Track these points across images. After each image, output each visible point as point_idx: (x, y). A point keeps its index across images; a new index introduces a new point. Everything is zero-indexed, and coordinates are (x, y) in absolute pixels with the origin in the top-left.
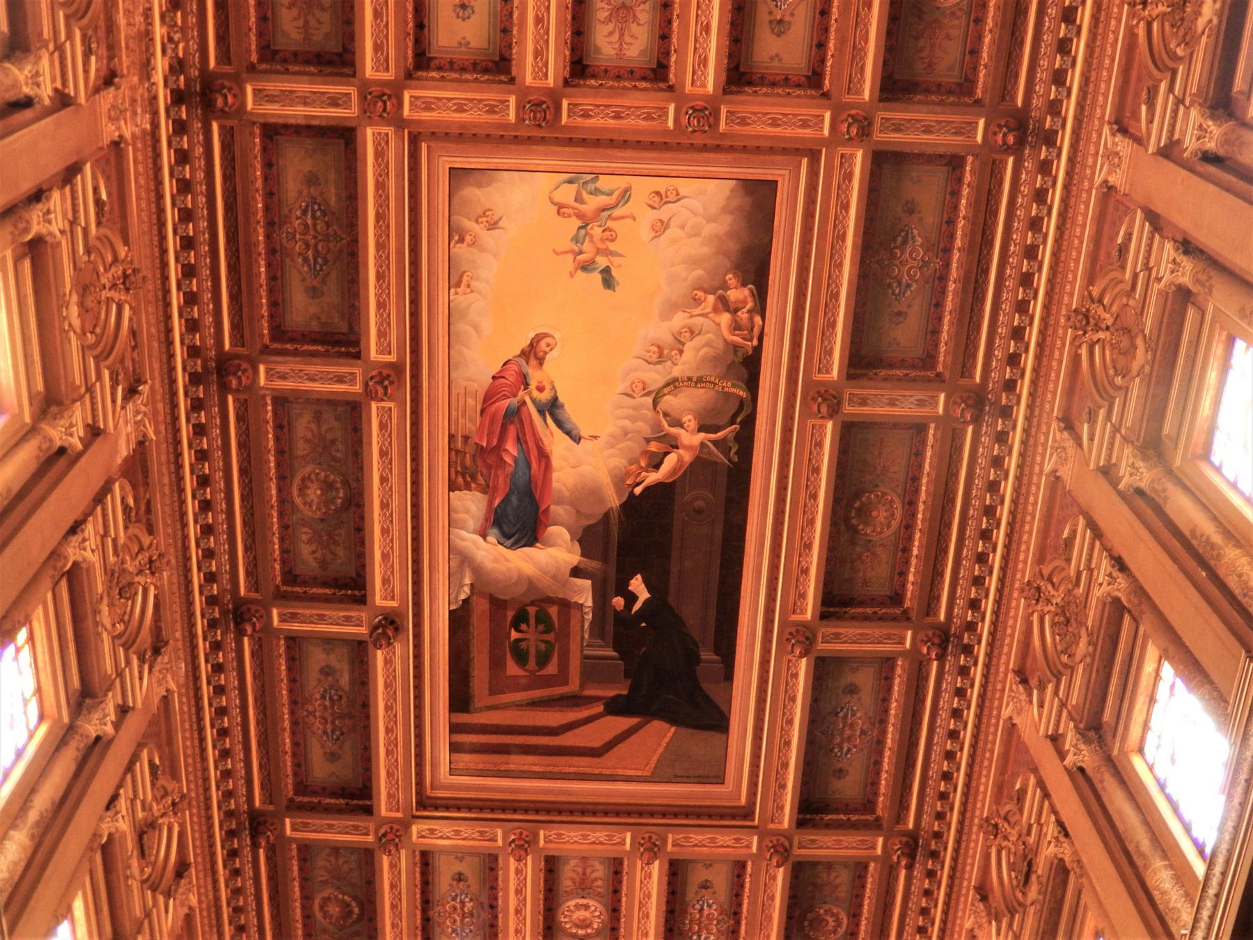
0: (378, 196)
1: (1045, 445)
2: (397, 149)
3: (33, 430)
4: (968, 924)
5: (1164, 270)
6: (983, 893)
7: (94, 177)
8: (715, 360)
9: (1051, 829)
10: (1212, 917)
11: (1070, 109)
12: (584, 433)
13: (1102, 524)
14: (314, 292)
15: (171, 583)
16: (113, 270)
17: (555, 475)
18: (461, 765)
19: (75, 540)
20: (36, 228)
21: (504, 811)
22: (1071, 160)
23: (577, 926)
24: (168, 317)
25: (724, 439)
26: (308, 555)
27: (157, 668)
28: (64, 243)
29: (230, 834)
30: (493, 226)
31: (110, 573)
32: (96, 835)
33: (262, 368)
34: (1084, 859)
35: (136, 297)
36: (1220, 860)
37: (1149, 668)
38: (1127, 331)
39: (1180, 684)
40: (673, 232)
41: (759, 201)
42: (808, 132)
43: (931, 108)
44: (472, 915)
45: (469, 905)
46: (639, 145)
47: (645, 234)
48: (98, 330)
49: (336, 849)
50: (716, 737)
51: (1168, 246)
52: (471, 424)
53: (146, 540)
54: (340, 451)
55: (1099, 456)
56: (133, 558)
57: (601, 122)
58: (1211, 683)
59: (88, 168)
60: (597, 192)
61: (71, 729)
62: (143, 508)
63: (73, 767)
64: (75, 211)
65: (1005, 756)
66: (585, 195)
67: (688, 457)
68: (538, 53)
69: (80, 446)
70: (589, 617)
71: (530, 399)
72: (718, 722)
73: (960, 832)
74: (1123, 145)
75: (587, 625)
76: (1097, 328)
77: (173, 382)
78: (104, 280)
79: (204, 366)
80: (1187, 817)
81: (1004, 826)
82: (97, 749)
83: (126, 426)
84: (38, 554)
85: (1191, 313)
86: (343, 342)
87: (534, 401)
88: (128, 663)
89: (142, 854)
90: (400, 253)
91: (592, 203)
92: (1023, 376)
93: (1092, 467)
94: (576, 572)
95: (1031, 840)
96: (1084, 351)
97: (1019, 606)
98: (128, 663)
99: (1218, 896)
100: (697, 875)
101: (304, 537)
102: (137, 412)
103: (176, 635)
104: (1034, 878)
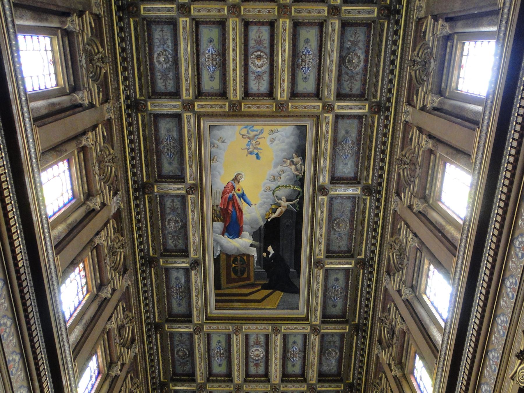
0: (188, 134)
1: (391, 201)
2: (193, 120)
3: (84, 203)
4: (376, 352)
5: (423, 144)
6: (380, 342)
7: (102, 129)
8: (291, 180)
9: (399, 320)
10: (448, 340)
11: (394, 100)
12: (252, 203)
13: (409, 224)
14: (170, 164)
15: (129, 252)
16: (109, 157)
17: (244, 216)
18: (219, 306)
19: (98, 237)
20: (84, 143)
21: (232, 320)
22: (395, 115)
23: (256, 357)
24: (127, 172)
25: (294, 203)
27: (125, 278)
28: (93, 148)
29: (148, 330)
30: (223, 142)
31: (109, 248)
32: (105, 328)
33: (155, 187)
34: (409, 328)
35: (117, 165)
36: (449, 320)
37: (426, 267)
38: (414, 164)
39: (436, 271)
40: (276, 142)
41: (302, 131)
42: (315, 110)
43: (351, 101)
44: (223, 354)
45: (222, 351)
46: (265, 116)
47: (268, 143)
48: (105, 175)
49: (181, 334)
50: (296, 295)
51: (424, 137)
52: (218, 201)
53: (121, 238)
54: (179, 211)
55: (407, 202)
56: (117, 244)
57: (254, 109)
58: (445, 268)
59: (100, 125)
60: (253, 131)
61: (97, 296)
62: (120, 229)
63: (97, 307)
64: (96, 138)
65: (384, 298)
66: (250, 132)
67: (284, 209)
68: (234, 90)
69: (99, 209)
70: (256, 259)
71: (236, 193)
72: (297, 291)
73: (372, 323)
74: (410, 109)
75: (255, 262)
76: (405, 164)
77: (129, 191)
78: (106, 160)
79: (138, 186)
80: (440, 312)
81: (385, 320)
82: (105, 302)
83: (114, 204)
84: (86, 240)
85: (432, 156)
86: (180, 178)
87: (237, 194)
88: (115, 275)
89: (120, 336)
90: (196, 151)
91: (252, 134)
92: (384, 181)
93: (405, 206)
94: (251, 246)
95: (394, 323)
96: (401, 171)
97: (386, 251)
98: (115, 275)
99: (449, 332)
100: (291, 340)
101: (170, 238)
102: (118, 200)
103: (131, 268)
104: (395, 336)
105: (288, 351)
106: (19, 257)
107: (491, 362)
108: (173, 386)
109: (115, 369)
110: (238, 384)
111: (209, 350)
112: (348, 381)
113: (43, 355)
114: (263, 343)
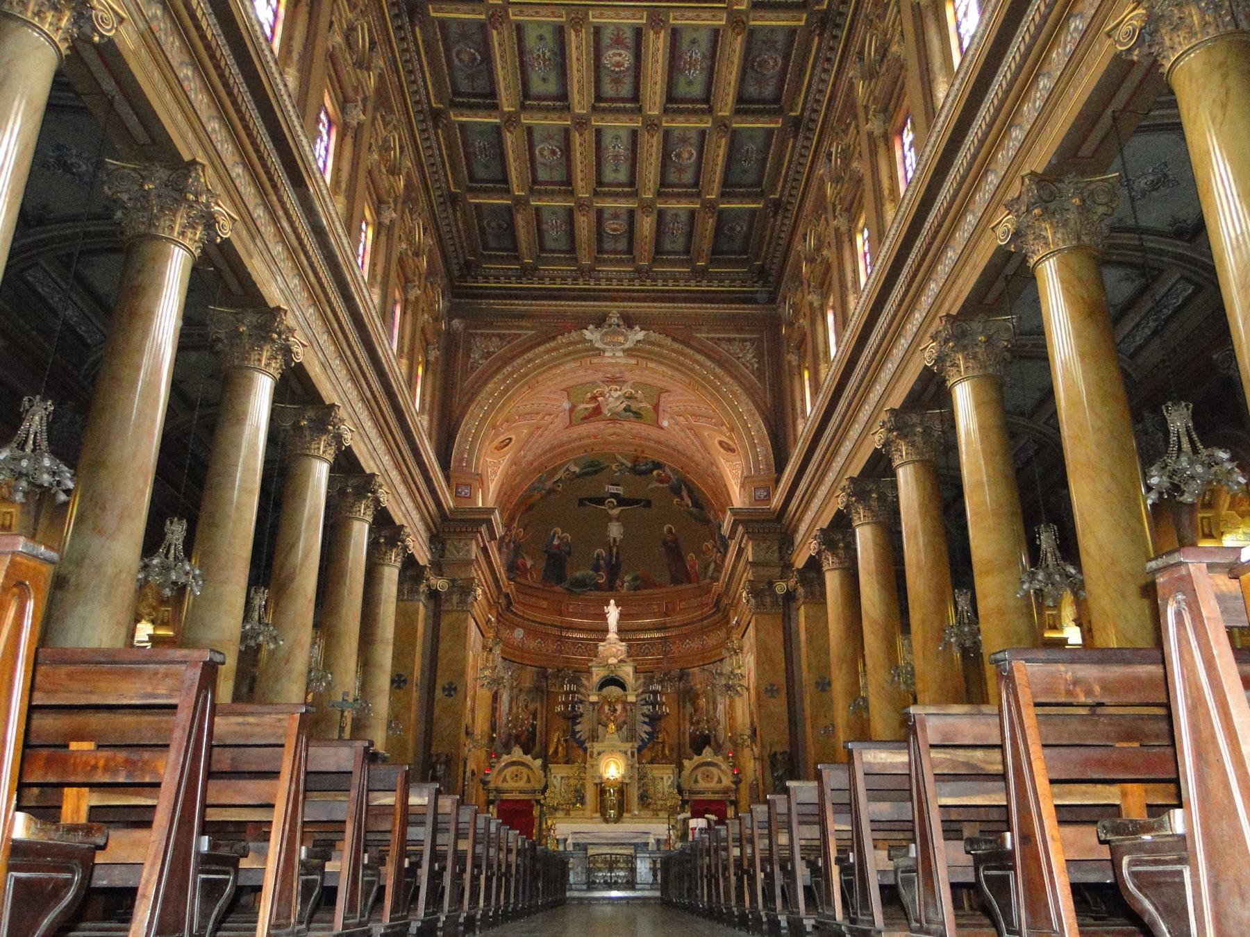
26: (464, 86)
45: (548, 54)
89: (350, 48)
97: (861, 28)
100: (686, 39)
105: (681, 57)
106: (204, 24)
108: (456, 116)
109: (354, 113)
110: (580, 116)
111: (521, 53)
112: (793, 114)
113: (274, 159)
114: (629, 42)
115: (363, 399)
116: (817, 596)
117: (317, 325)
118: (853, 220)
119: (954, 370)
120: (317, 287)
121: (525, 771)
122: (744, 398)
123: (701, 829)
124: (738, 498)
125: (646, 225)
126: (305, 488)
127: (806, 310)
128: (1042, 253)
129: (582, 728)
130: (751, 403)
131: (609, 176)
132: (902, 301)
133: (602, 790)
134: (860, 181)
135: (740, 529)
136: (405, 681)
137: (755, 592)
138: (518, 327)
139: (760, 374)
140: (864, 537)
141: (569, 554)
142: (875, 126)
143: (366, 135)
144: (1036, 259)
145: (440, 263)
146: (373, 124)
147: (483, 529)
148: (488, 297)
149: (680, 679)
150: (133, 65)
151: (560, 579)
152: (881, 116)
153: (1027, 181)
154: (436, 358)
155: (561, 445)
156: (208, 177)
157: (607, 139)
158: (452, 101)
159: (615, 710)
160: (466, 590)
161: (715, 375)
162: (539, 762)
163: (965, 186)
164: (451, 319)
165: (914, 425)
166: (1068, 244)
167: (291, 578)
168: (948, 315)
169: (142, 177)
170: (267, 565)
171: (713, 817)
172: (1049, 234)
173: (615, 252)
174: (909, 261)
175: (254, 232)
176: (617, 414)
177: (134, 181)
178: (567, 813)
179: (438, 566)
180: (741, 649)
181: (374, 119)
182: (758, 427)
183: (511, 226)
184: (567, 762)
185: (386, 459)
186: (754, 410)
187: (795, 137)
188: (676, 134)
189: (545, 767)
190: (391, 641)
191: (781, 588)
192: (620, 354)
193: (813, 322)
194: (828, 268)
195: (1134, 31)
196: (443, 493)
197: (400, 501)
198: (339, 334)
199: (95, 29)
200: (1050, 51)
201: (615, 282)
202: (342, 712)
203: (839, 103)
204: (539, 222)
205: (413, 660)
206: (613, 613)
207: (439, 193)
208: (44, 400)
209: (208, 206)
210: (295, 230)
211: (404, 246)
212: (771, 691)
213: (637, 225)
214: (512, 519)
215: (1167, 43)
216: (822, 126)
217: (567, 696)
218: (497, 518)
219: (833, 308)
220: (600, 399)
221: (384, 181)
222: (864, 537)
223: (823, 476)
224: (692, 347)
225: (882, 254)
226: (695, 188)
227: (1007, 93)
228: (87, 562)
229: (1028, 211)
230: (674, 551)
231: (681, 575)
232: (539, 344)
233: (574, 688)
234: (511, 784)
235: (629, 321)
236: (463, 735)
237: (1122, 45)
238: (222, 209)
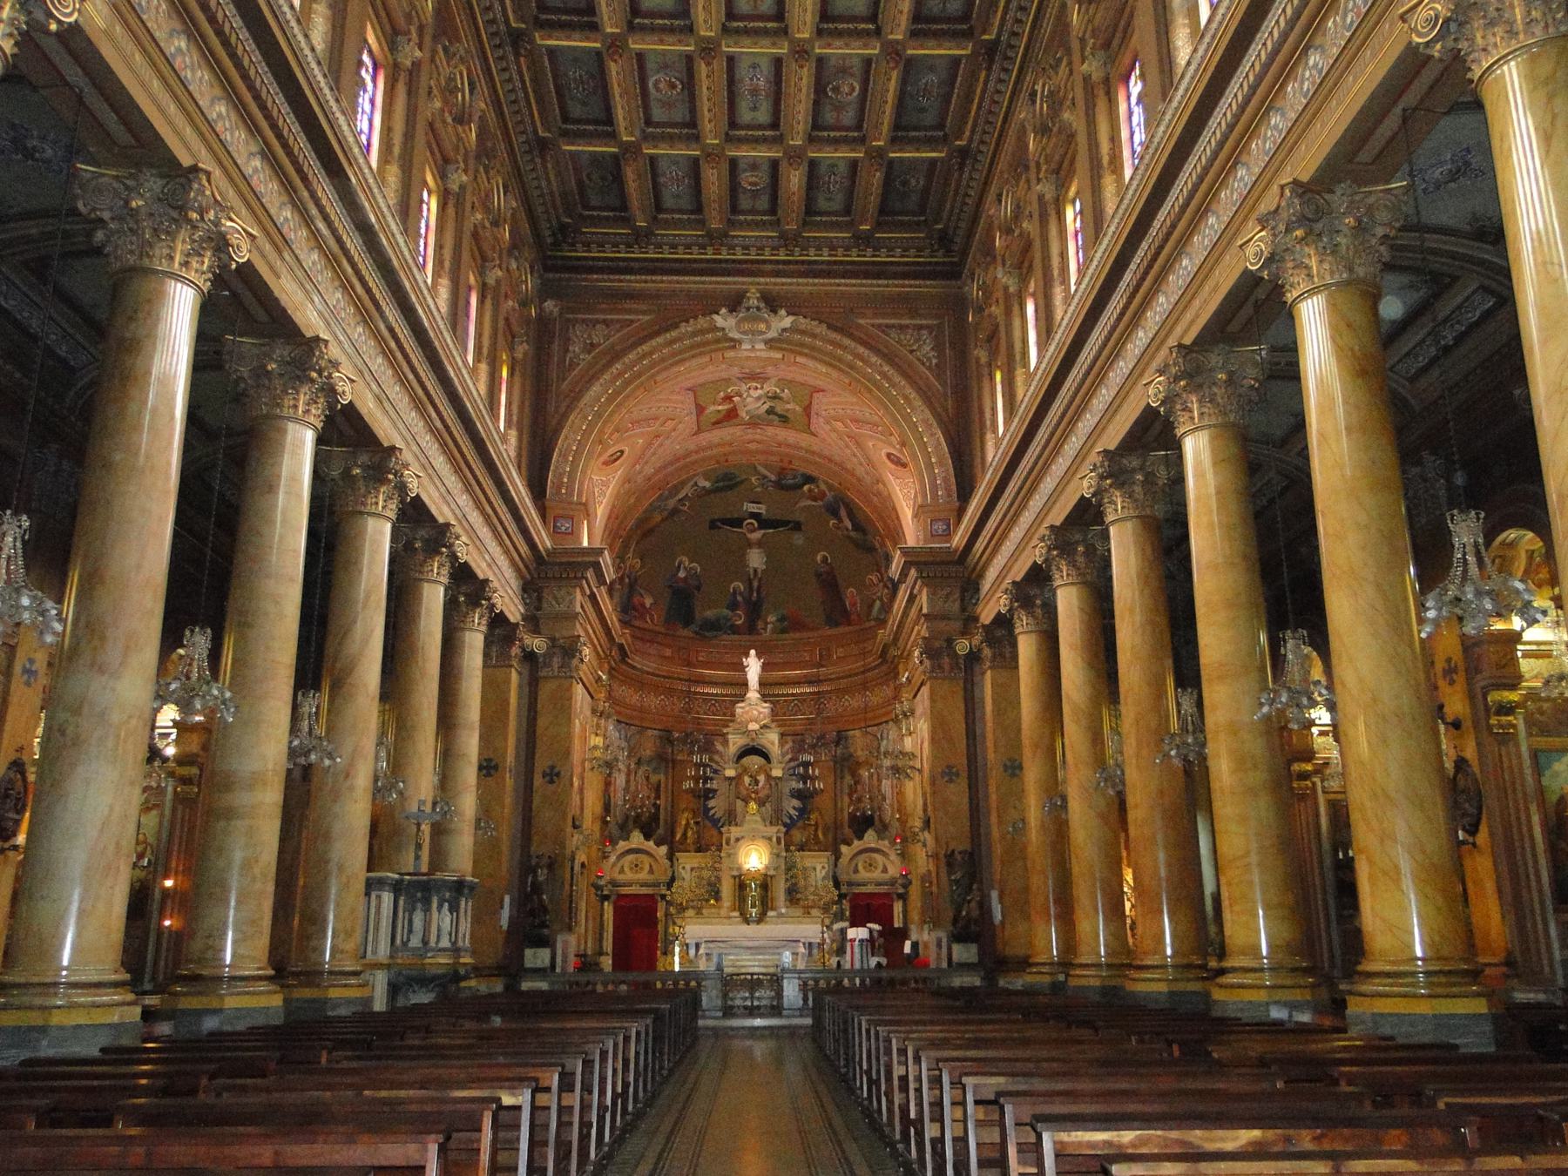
107: (1307, 74)
109: (407, 49)
110: (708, 40)
112: (986, 37)
115: (432, 430)
116: (1007, 659)
117: (368, 346)
118: (1062, 185)
119: (1187, 415)
120: (365, 298)
121: (645, 859)
122: (918, 403)
123: (861, 941)
124: (912, 533)
125: (794, 180)
126: (359, 552)
127: (999, 294)
128: (1303, 287)
129: (717, 805)
130: (927, 411)
131: (745, 116)
132: (1122, 314)
133: (741, 885)
134: (1072, 136)
135: (913, 573)
136: (496, 767)
137: (930, 652)
138: (629, 311)
139: (939, 370)
140: (1068, 600)
141: (698, 588)
142: (1092, 67)
143: (424, 78)
144: (1295, 294)
145: (525, 227)
146: (433, 60)
147: (590, 574)
148: (591, 270)
149: (837, 744)
150: (107, 52)
151: (688, 620)
152: (1101, 54)
153: (1287, 192)
154: (525, 354)
155: (688, 454)
156: (218, 184)
157: (743, 71)
158: (536, 18)
159: (757, 782)
160: (569, 651)
161: (884, 375)
162: (664, 849)
163: (1208, 179)
164: (543, 301)
165: (1134, 471)
166: (1337, 278)
167: (349, 670)
168: (1180, 346)
169: (127, 188)
170: (316, 663)
171: (876, 927)
172: (1314, 263)
173: (753, 212)
174: (1133, 266)
175: (281, 242)
176: (759, 417)
177: (117, 194)
178: (699, 912)
179: (533, 621)
180: (913, 713)
181: (434, 52)
182: (936, 441)
183: (618, 179)
184: (698, 850)
185: (464, 500)
186: (932, 420)
187: (989, 69)
188: (833, 62)
189: (671, 857)
190: (477, 725)
191: (963, 646)
192: (761, 346)
193: (1008, 313)
194: (1028, 247)
195: (1437, 17)
196: (538, 533)
197: (481, 547)
198: (399, 355)
199: (50, 15)
200: (1324, 19)
201: (753, 251)
202: (419, 825)
203: (1048, 26)
204: (655, 175)
205: (506, 740)
206: (753, 667)
207: (523, 138)
208: (16, 513)
209: (217, 223)
210: (334, 231)
211: (479, 216)
212: (949, 773)
213: (782, 183)
214: (625, 546)
215: (1479, 40)
216: (1025, 56)
217: (697, 770)
218: (606, 560)
219: (1033, 295)
220: (736, 399)
221: (448, 133)
222: (1068, 600)
223: (1017, 515)
224: (851, 336)
225: (1099, 255)
226: (858, 133)
227: (1266, 67)
228: (86, 710)
229: (1288, 230)
230: (830, 584)
231: (837, 613)
232: (657, 333)
233: (706, 758)
234: (629, 875)
235: (772, 303)
236: (569, 829)
237: (1420, 35)
238: (237, 226)
